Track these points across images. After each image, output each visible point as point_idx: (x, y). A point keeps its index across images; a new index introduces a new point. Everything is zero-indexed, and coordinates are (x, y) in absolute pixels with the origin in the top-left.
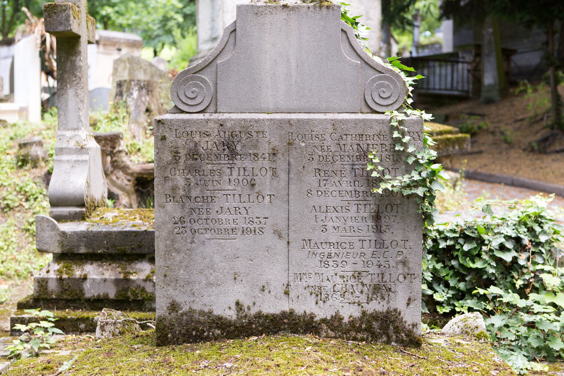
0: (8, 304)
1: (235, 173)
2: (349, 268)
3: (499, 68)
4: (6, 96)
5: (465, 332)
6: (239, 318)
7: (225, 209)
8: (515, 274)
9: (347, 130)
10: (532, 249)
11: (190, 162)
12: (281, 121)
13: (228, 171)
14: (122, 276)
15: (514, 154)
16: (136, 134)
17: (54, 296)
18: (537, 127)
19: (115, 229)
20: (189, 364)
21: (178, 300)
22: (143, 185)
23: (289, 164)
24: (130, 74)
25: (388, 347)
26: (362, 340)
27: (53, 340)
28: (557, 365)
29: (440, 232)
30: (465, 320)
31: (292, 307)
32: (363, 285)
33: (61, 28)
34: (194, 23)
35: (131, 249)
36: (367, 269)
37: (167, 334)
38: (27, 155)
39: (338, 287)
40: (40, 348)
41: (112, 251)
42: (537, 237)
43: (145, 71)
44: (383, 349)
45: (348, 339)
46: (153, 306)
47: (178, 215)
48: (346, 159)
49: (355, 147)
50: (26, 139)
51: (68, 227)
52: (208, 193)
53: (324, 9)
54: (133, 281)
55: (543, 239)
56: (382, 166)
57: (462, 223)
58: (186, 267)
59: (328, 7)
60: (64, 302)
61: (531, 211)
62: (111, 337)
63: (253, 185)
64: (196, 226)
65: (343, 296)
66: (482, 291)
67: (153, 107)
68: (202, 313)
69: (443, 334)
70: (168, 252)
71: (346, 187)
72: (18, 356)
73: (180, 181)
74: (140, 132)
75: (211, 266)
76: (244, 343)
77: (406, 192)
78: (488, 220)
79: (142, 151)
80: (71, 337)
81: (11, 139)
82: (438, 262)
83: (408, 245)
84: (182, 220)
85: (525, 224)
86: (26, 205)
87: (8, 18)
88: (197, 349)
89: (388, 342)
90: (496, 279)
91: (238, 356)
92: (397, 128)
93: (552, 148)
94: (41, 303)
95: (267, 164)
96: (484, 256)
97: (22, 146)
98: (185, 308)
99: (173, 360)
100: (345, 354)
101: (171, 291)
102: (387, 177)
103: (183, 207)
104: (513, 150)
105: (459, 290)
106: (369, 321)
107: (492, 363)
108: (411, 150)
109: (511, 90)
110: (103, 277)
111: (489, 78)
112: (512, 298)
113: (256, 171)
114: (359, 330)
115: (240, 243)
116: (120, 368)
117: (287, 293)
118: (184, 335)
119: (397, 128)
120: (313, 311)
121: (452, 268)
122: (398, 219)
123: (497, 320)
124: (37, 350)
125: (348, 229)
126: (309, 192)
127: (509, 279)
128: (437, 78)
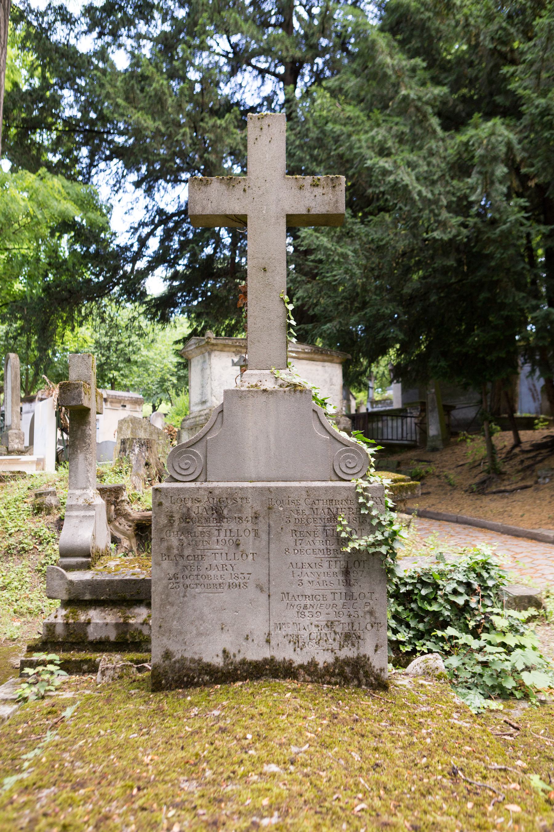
0: (19, 641)
1: (222, 534)
2: (322, 619)
3: (441, 422)
4: (26, 447)
5: (427, 673)
6: (226, 665)
7: (214, 566)
8: (467, 616)
9: (319, 496)
10: (482, 593)
11: (183, 525)
12: (262, 489)
13: (216, 533)
14: (122, 620)
15: (457, 495)
16: (137, 485)
17: (60, 640)
18: (475, 471)
19: (117, 578)
20: (180, 713)
21: (171, 648)
22: (142, 530)
23: (269, 526)
24: (132, 432)
25: (359, 690)
26: (336, 684)
27: (57, 682)
28: (511, 703)
29: (400, 579)
30: (426, 662)
31: (272, 654)
32: (335, 633)
33: (73, 403)
34: (187, 384)
35: (129, 595)
36: (339, 619)
37: (161, 681)
38: (42, 504)
39: (314, 636)
40: (46, 691)
41: (113, 597)
42: (484, 581)
43: (145, 429)
44: (355, 693)
45: (323, 683)
46: (149, 647)
47: (172, 572)
48: (319, 521)
49: (326, 511)
50: (43, 489)
51: (75, 576)
52: (199, 552)
53: (298, 393)
54: (132, 625)
55: (490, 583)
56: (350, 527)
57: (419, 570)
58: (179, 618)
59: (301, 391)
60: (68, 645)
61: (479, 558)
62: (110, 682)
63: (238, 545)
64: (188, 581)
65: (318, 643)
66: (439, 633)
67: (152, 461)
68: (192, 660)
69: (407, 674)
70: (163, 605)
71: (319, 545)
72: (25, 699)
73: (174, 542)
74: (140, 484)
75: (201, 618)
76: (231, 689)
77: (372, 550)
78: (442, 567)
79: (141, 501)
80: (75, 677)
81: (29, 489)
82: (399, 605)
83: (374, 596)
84: (175, 576)
85: (474, 570)
86: (40, 548)
87: (31, 379)
88: (188, 695)
89: (359, 686)
90: (451, 620)
91: (225, 703)
92: (362, 494)
93: (489, 490)
94: (49, 645)
95: (250, 526)
96: (440, 600)
97: (38, 495)
98: (178, 657)
99: (166, 707)
100: (321, 699)
101: (165, 641)
102: (355, 537)
103: (177, 564)
104: (456, 491)
105: (418, 630)
106: (341, 667)
107: (452, 705)
108: (374, 513)
109: (452, 440)
110: (105, 621)
111: (433, 430)
112: (465, 638)
113: (241, 533)
114: (333, 675)
115: (225, 596)
116: (118, 716)
117: (268, 641)
118: (176, 681)
119: (362, 494)
120: (291, 657)
121: (412, 610)
122: (365, 574)
123: (454, 661)
124: (42, 692)
125: (321, 582)
126: (287, 550)
127: (462, 620)
128: (390, 430)
